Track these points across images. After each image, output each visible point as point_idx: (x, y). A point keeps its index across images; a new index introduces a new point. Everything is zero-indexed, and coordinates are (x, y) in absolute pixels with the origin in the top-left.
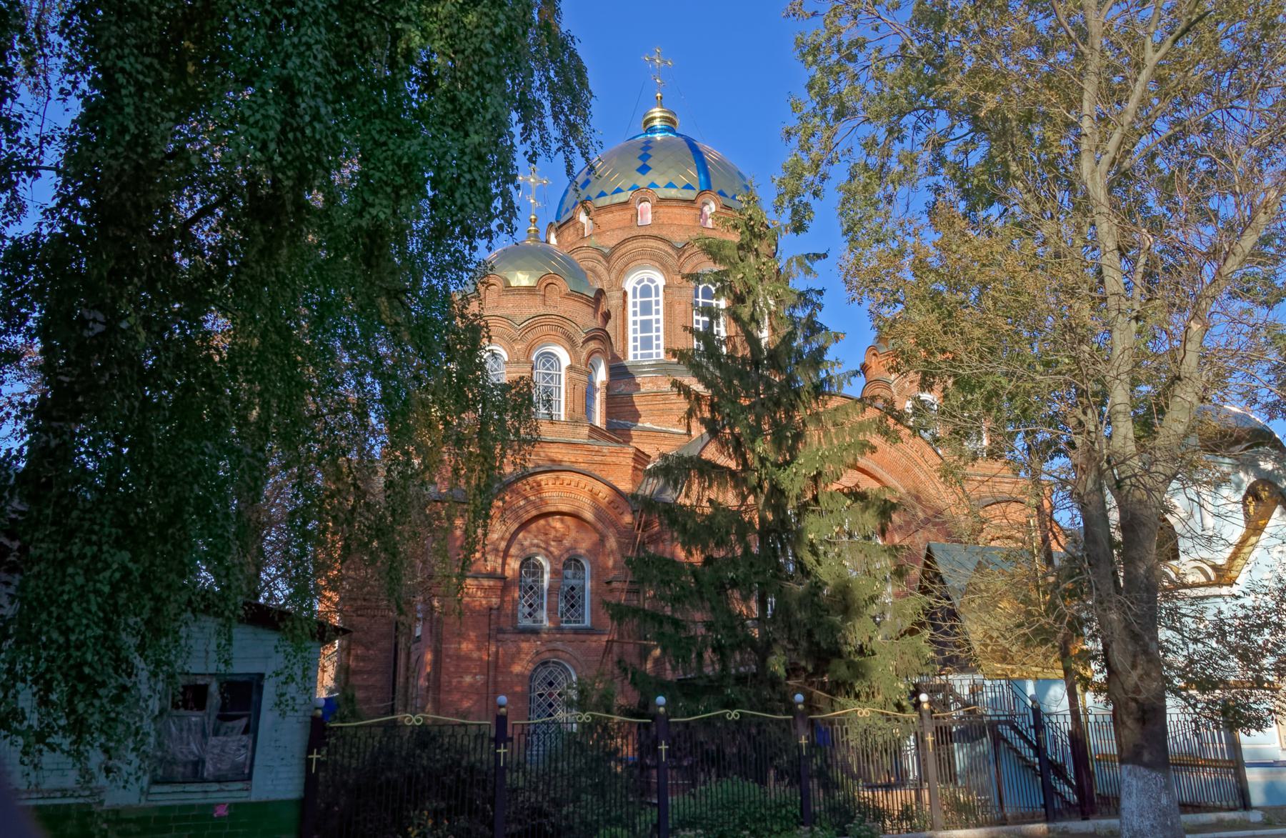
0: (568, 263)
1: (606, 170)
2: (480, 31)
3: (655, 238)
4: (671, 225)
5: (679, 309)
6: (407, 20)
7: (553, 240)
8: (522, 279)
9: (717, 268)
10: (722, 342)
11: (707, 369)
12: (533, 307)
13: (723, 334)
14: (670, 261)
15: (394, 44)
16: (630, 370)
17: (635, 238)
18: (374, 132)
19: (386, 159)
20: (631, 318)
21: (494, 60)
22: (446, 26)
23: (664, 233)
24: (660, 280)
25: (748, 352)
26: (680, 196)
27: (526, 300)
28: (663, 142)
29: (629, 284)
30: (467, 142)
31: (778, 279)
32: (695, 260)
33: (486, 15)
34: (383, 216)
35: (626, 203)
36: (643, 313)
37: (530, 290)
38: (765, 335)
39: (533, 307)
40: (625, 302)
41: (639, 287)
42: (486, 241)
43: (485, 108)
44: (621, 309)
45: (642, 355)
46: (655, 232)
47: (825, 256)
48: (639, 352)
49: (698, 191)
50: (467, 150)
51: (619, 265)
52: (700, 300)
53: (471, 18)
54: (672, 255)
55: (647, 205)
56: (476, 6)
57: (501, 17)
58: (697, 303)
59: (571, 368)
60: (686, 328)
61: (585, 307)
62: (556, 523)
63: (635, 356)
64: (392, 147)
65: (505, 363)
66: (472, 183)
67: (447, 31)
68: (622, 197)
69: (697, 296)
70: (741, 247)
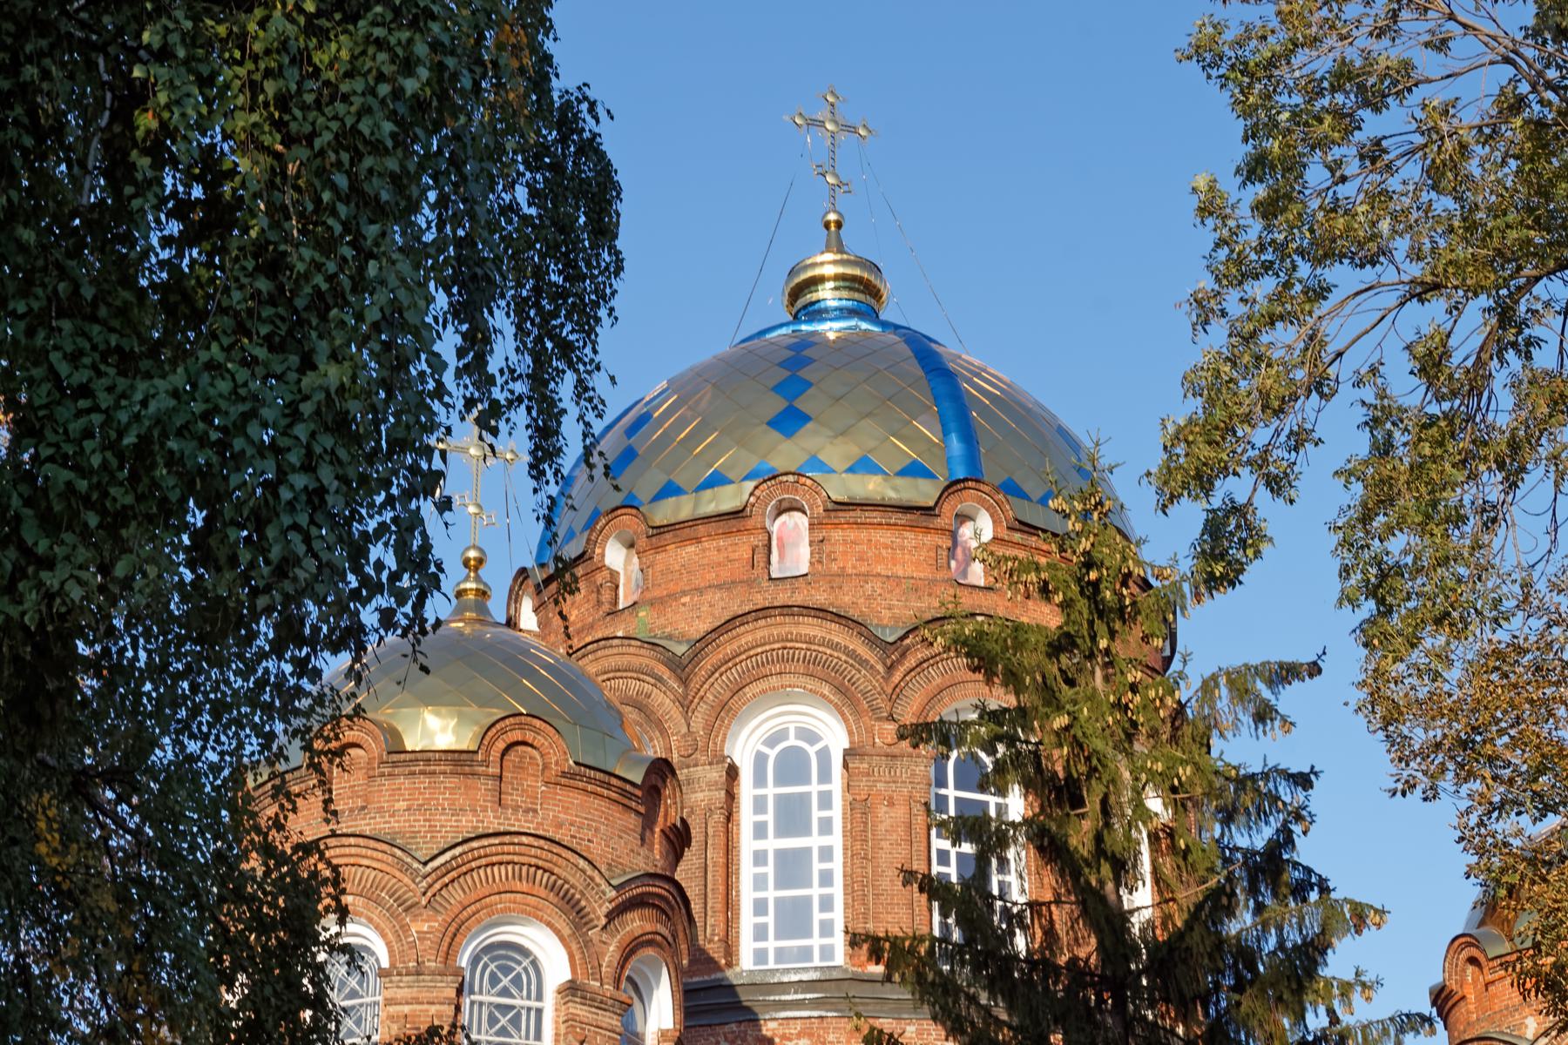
0: (570, 684)
1: (682, 423)
2: (359, 84)
3: (821, 612)
4: (866, 576)
5: (889, 818)
6: (163, 54)
7: (528, 619)
8: (435, 730)
9: (1001, 698)
10: (1014, 920)
11: (973, 999)
12: (460, 812)
13: (1018, 897)
14: (864, 681)
15: (124, 116)
16: (745, 997)
17: (763, 612)
18: (55, 357)
19: (88, 434)
20: (747, 845)
21: (392, 164)
22: (268, 73)
23: (845, 600)
24: (835, 735)
25: (1088, 949)
26: (891, 495)
27: (448, 788)
28: (845, 344)
29: (745, 744)
30: (308, 380)
31: (1174, 739)
32: (936, 677)
33: (380, 44)
34: (76, 593)
35: (737, 514)
36: (781, 832)
37: (458, 760)
38: (1141, 900)
39: (460, 812)
40: (731, 796)
41: (772, 754)
42: (345, 658)
43: (360, 284)
44: (718, 817)
45: (781, 954)
46: (820, 598)
47: (1315, 669)
48: (771, 944)
49: (943, 482)
50: (307, 408)
51: (716, 689)
52: (951, 792)
53: (341, 48)
54: (862, 658)
55: (796, 523)
56: (354, 18)
57: (421, 49)
58: (941, 801)
59: (571, 990)
60: (908, 876)
61: (616, 812)
62: (980, 618)
63: (760, 956)
64: (105, 400)
65: (383, 973)
66: (316, 497)
67: (270, 87)
68: (727, 499)
69: (941, 782)
70: (1061, 644)
